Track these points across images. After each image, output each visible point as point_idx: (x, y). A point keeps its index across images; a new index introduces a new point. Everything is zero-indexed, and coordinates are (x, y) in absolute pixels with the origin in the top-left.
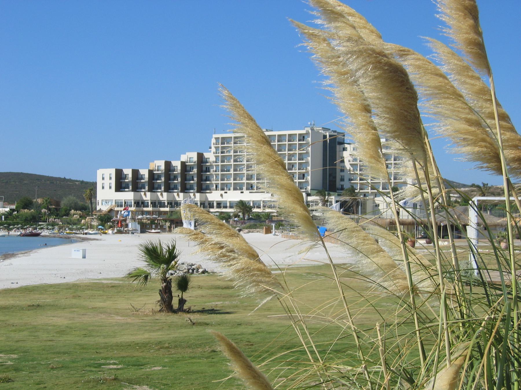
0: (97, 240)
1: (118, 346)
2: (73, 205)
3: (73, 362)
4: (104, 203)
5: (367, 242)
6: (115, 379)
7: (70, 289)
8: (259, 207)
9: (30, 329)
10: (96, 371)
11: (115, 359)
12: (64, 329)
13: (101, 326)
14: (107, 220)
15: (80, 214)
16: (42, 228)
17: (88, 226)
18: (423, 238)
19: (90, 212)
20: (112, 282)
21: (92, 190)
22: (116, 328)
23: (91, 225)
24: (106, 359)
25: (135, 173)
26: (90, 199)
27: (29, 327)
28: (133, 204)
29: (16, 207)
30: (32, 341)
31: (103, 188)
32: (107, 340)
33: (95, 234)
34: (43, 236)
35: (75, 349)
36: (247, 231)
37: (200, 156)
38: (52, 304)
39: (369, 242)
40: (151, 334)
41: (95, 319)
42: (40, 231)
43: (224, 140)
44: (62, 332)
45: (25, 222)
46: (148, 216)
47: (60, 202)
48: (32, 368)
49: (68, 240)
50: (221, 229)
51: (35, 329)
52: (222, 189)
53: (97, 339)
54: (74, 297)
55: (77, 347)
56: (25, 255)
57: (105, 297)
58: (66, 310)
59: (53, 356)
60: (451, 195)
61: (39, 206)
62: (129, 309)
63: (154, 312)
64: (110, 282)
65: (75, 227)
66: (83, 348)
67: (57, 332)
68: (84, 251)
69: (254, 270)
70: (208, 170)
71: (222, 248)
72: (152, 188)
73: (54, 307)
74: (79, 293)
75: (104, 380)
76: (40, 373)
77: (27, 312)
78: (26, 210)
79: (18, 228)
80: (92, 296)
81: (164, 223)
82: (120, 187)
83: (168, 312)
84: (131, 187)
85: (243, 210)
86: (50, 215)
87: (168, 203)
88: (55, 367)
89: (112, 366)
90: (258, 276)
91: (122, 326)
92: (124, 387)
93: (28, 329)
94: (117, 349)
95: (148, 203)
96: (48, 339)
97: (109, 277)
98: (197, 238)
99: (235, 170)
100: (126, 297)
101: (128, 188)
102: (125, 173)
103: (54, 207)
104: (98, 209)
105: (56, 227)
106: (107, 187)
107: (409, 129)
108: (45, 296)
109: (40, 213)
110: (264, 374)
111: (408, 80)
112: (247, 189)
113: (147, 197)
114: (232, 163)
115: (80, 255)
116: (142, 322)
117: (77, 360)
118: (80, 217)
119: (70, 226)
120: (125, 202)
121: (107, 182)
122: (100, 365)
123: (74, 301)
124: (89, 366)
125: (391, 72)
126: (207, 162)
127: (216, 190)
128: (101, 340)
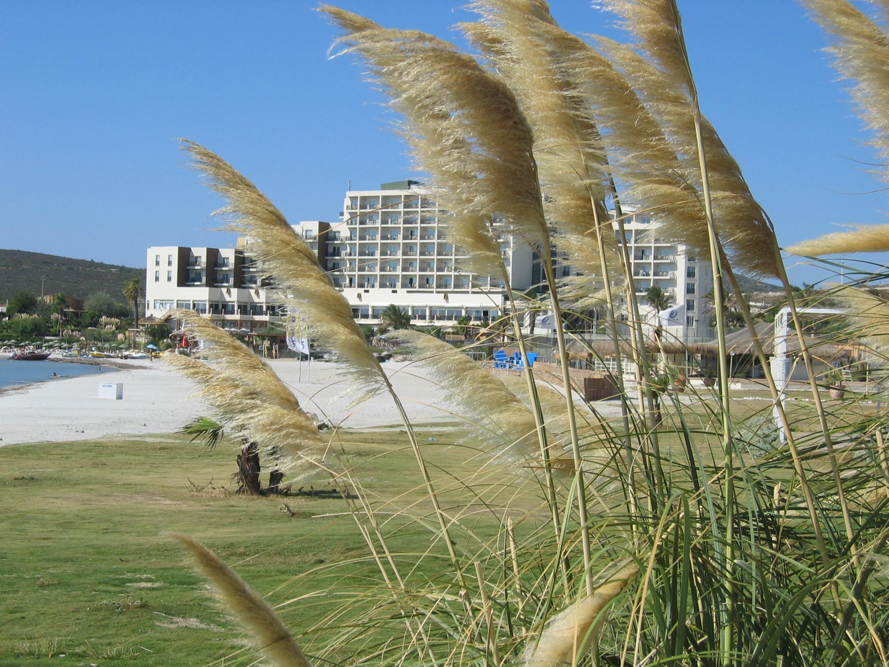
0: (145, 368)
1: (159, 550)
2: (104, 307)
3: (79, 576)
4: (158, 305)
5: (489, 386)
6: (143, 606)
7: (90, 451)
8: (423, 317)
9: (13, 518)
10: (115, 592)
11: (151, 571)
12: (72, 520)
13: (134, 516)
14: (163, 335)
15: (117, 323)
16: (51, 347)
17: (130, 344)
18: (699, 375)
19: (133, 320)
20: (163, 440)
21: (137, 282)
22: (160, 519)
23: (135, 342)
24: (135, 571)
25: (213, 255)
26: (135, 299)
27: (12, 515)
28: (207, 307)
29: (8, 310)
30: (14, 539)
31: (157, 279)
32: (141, 540)
33: (141, 358)
34: (52, 360)
35: (85, 553)
36: (400, 357)
37: (324, 226)
38: (56, 476)
39: (493, 386)
40: (220, 530)
41: (125, 503)
42: (47, 352)
43: (365, 202)
44: (67, 524)
45: (22, 335)
46: (233, 329)
47: (83, 302)
48: (9, 584)
49: (96, 367)
50: (236, 355)
51: (22, 518)
52: (361, 286)
53: (125, 537)
54: (95, 465)
55: (90, 550)
56: (20, 391)
57: (147, 467)
58: (78, 486)
59: (47, 565)
60: (751, 303)
61: (47, 309)
62: (187, 487)
63: (228, 494)
64: (159, 440)
65: (107, 345)
66: (99, 553)
67: (58, 525)
68: (120, 387)
69: (288, 426)
70: (337, 252)
71: (236, 387)
72: (241, 282)
73: (58, 481)
74: (104, 459)
75: (124, 607)
76: (20, 594)
77: (10, 489)
78: (24, 316)
79: (10, 346)
80: (126, 464)
81: (259, 342)
82: (186, 278)
83: (252, 494)
84: (204, 279)
85: (396, 322)
86: (66, 323)
87: (268, 308)
88: (46, 583)
89: (143, 585)
90: (296, 437)
91: (171, 516)
92: (157, 620)
93: (9, 518)
94: (156, 555)
95: (233, 306)
96: (43, 535)
97: (158, 432)
98: (197, 373)
99: (383, 253)
100: (184, 466)
101: (200, 280)
102: (195, 255)
103: (72, 310)
104: (148, 315)
105: (75, 345)
106: (163, 277)
107: (519, 193)
108: (45, 463)
109: (48, 320)
110: (269, 605)
111: (515, 109)
112: (403, 286)
113: (233, 296)
114: (378, 241)
115: (112, 393)
116: (206, 511)
117: (87, 572)
118: (117, 329)
119: (100, 344)
120: (194, 305)
121: (163, 269)
122: (124, 582)
123: (94, 472)
124: (104, 583)
125: (486, 96)
126: (335, 239)
127: (351, 286)
128: (132, 539)
